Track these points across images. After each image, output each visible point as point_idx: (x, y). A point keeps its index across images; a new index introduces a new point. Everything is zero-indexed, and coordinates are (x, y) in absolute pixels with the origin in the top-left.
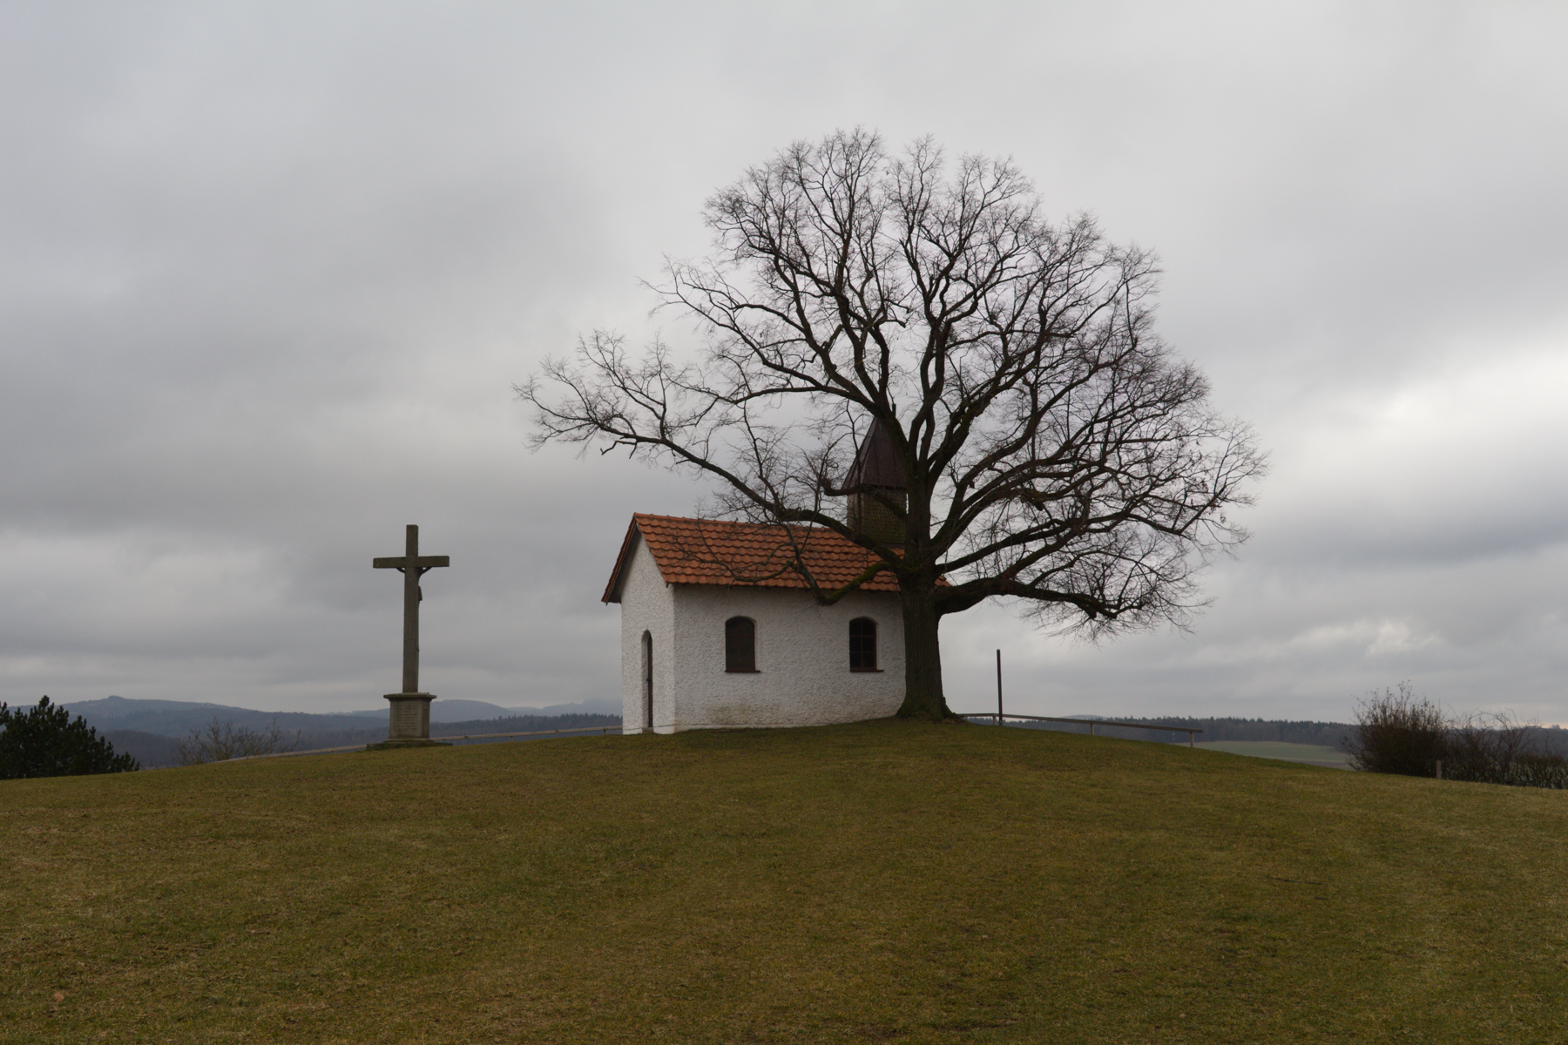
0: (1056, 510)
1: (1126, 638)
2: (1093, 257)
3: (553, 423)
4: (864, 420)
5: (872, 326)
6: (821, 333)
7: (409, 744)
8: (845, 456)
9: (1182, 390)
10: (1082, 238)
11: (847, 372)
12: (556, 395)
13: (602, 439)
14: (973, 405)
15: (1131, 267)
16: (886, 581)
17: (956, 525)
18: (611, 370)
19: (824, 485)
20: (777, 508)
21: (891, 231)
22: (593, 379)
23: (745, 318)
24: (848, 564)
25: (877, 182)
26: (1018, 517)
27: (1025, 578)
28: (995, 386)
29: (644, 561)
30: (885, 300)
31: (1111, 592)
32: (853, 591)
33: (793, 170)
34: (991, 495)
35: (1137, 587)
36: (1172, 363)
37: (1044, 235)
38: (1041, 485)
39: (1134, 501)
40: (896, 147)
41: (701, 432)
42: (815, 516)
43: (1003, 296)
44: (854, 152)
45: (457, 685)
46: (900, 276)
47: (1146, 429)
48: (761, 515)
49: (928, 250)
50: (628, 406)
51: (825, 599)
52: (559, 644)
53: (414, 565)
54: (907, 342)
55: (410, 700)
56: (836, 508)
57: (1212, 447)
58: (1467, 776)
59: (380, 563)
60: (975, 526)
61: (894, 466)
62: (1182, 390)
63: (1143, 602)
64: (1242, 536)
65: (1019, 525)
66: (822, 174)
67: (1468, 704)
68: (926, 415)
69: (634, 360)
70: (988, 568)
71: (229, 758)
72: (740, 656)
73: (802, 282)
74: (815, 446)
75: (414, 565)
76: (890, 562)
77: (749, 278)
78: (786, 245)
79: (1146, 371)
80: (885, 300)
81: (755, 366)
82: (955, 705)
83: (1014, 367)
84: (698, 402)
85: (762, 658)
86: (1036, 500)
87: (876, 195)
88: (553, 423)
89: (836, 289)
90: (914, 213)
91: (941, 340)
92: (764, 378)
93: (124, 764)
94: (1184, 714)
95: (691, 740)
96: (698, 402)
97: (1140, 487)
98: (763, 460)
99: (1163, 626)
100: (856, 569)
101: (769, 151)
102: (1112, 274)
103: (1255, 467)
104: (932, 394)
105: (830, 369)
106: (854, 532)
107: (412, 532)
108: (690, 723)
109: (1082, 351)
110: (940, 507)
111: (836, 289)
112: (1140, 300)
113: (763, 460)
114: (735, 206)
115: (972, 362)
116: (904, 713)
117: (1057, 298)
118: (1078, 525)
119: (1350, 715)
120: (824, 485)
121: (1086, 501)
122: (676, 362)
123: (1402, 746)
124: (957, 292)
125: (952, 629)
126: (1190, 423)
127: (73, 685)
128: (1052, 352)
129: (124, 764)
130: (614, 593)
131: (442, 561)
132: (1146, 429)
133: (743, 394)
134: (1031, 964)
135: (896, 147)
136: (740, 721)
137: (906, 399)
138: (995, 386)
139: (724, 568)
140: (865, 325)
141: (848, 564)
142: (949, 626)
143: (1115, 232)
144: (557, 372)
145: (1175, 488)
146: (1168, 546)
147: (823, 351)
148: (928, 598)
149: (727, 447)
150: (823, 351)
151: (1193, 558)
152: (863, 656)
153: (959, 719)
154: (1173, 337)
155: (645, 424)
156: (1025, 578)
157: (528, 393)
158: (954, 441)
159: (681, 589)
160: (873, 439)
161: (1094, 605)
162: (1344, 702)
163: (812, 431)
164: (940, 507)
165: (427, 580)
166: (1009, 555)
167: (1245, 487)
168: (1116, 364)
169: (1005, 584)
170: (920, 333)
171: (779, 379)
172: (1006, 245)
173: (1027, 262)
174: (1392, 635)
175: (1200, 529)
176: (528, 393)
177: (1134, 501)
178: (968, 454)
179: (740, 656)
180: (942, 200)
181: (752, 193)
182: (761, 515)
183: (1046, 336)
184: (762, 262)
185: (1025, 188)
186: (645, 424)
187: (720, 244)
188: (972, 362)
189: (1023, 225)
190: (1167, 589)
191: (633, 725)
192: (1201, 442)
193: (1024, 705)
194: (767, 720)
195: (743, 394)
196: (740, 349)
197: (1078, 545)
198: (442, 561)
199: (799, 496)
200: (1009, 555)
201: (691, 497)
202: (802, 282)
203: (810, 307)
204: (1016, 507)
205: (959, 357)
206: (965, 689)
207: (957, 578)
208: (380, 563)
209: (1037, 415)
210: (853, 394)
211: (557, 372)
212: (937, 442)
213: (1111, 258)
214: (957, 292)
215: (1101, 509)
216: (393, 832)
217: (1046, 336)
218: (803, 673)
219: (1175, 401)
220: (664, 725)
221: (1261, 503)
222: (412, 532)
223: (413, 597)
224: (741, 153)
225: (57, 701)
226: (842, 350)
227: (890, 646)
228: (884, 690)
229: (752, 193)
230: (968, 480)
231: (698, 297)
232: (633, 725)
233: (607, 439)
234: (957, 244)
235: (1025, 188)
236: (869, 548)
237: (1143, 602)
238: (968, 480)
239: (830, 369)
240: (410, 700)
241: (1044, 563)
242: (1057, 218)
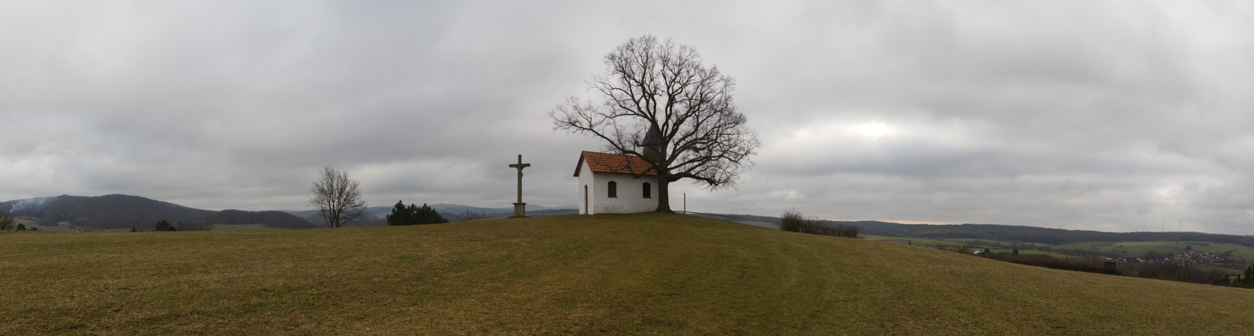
0: (702, 153)
1: (720, 191)
2: (717, 78)
3: (559, 124)
4: (649, 124)
5: (652, 96)
6: (637, 98)
7: (519, 217)
8: (643, 135)
9: (739, 120)
10: (714, 72)
11: (644, 110)
12: (560, 115)
13: (573, 129)
14: (680, 121)
15: (727, 82)
16: (653, 172)
17: (674, 156)
18: (576, 108)
19: (636, 144)
20: (623, 150)
21: (658, 67)
22: (571, 110)
23: (614, 92)
24: (641, 167)
25: (655, 51)
26: (691, 155)
27: (693, 173)
28: (687, 116)
29: (585, 165)
30: (656, 88)
31: (717, 178)
32: (644, 175)
33: (630, 47)
34: (685, 148)
35: (724, 177)
36: (737, 112)
37: (703, 70)
38: (698, 146)
39: (725, 152)
40: (661, 41)
41: (601, 127)
42: (633, 152)
43: (690, 88)
44: (648, 41)
45: (533, 201)
46: (661, 81)
47: (729, 131)
48: (618, 152)
49: (669, 73)
50: (581, 119)
51: (636, 177)
52: (563, 189)
53: (520, 166)
54: (662, 101)
55: (520, 204)
56: (640, 150)
57: (747, 137)
58: (807, 232)
59: (511, 166)
60: (679, 157)
61: (657, 138)
62: (739, 120)
63: (725, 181)
64: (753, 164)
65: (692, 157)
66: (639, 48)
67: (810, 213)
68: (666, 123)
69: (583, 105)
70: (682, 169)
71: (472, 220)
72: (612, 192)
73: (632, 82)
74: (634, 132)
75: (520, 166)
76: (655, 167)
77: (616, 80)
78: (627, 70)
79: (730, 114)
80: (656, 88)
81: (617, 107)
82: (672, 209)
83: (692, 110)
84: (600, 118)
85: (618, 193)
86: (697, 150)
87: (654, 55)
88: (559, 124)
89: (642, 84)
90: (665, 62)
91: (672, 101)
92: (620, 111)
93: (445, 221)
94: (736, 213)
95: (598, 216)
96: (600, 118)
97: (726, 148)
98: (619, 136)
99: (731, 188)
100: (645, 168)
101: (623, 40)
102: (722, 84)
103: (758, 144)
104: (668, 117)
105: (639, 108)
106: (645, 158)
107: (520, 157)
108: (598, 211)
109: (712, 106)
110: (669, 151)
111: (642, 84)
112: (729, 92)
113: (619, 136)
114: (613, 58)
115: (680, 108)
116: (658, 210)
117: (706, 90)
118: (708, 158)
119: (779, 215)
120: (636, 144)
121: (711, 151)
122: (595, 106)
123: (792, 224)
124: (677, 86)
125: (672, 186)
126: (741, 130)
127: (433, 200)
128: (703, 106)
129: (445, 221)
130: (577, 174)
131: (528, 165)
132: (729, 131)
133: (614, 116)
134: (689, 279)
135: (661, 41)
136: (612, 211)
137: (661, 118)
138: (687, 116)
139: (608, 167)
140: (650, 96)
141: (641, 167)
142: (672, 186)
143: (724, 71)
144: (560, 108)
145: (736, 149)
146: (733, 166)
147: (637, 103)
148: (666, 178)
149: (609, 131)
150: (637, 103)
151: (740, 169)
152: (647, 194)
153: (683, 217)
154: (738, 104)
155: (586, 125)
156: (693, 173)
157: (552, 115)
158: (674, 132)
159: (595, 173)
160: (651, 130)
161: (712, 181)
162: (778, 212)
163: (633, 127)
164: (669, 151)
165: (524, 171)
166: (690, 165)
167: (755, 150)
168: (721, 111)
169: (687, 174)
170: (666, 98)
171: (624, 111)
172: (692, 73)
173: (697, 78)
174: (792, 194)
175: (742, 161)
176: (552, 115)
177: (725, 152)
178: (678, 136)
179: (612, 192)
180: (674, 58)
181: (618, 54)
182: (618, 152)
183: (702, 101)
184: (620, 75)
185: (698, 56)
186: (586, 125)
187: (608, 69)
188: (680, 108)
189: (697, 67)
190: (732, 178)
191: (582, 212)
192: (742, 136)
193: (691, 209)
194: (619, 211)
195: (614, 116)
196: (613, 102)
197: (708, 164)
198: (528, 165)
199: (629, 146)
200: (689, 166)
201: (599, 146)
202: (632, 82)
203: (634, 89)
204: (691, 152)
205: (676, 106)
206: (675, 204)
207: (674, 172)
208: (511, 166)
209: (698, 125)
210: (645, 116)
211: (560, 108)
212: (669, 132)
213: (722, 79)
214: (677, 86)
215: (715, 154)
216: (517, 240)
217: (702, 101)
218: (630, 198)
219: (737, 123)
220: (591, 212)
221: (760, 155)
222: (520, 157)
223: (520, 175)
224: (615, 41)
225: (407, 203)
226: (643, 103)
227: (654, 191)
228: (652, 203)
229: (618, 54)
230: (678, 143)
231: (601, 86)
232: (582, 212)
233: (574, 129)
234: (678, 71)
235: (698, 56)
236: (646, 163)
237: (725, 181)
238: (678, 143)
239: (639, 108)
240: (520, 204)
241: (698, 169)
242: (707, 66)
